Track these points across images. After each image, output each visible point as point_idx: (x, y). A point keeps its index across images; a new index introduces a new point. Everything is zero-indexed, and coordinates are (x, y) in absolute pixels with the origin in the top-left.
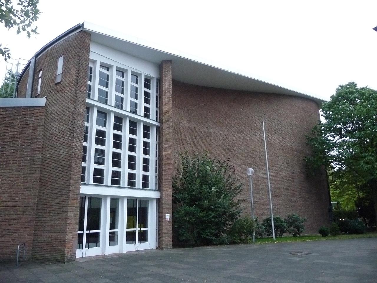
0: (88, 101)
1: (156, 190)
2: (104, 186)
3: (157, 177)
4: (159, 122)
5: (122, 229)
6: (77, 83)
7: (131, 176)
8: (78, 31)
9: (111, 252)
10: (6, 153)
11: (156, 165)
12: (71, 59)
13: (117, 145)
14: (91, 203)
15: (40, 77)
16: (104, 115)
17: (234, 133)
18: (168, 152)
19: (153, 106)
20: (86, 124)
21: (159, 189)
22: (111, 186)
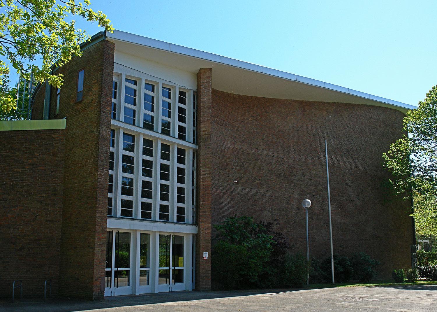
0: (113, 122)
1: (193, 224)
2: (152, 221)
3: (194, 209)
4: (197, 144)
5: (155, 266)
6: (100, 103)
7: (164, 209)
8: (100, 40)
9: (143, 292)
10: (26, 183)
11: (193, 176)
12: (93, 74)
13: (147, 173)
14: (119, 237)
15: (59, 94)
16: (131, 137)
17: (292, 155)
18: (206, 181)
19: (188, 125)
20: (112, 149)
21: (196, 222)
22: (160, 221)
